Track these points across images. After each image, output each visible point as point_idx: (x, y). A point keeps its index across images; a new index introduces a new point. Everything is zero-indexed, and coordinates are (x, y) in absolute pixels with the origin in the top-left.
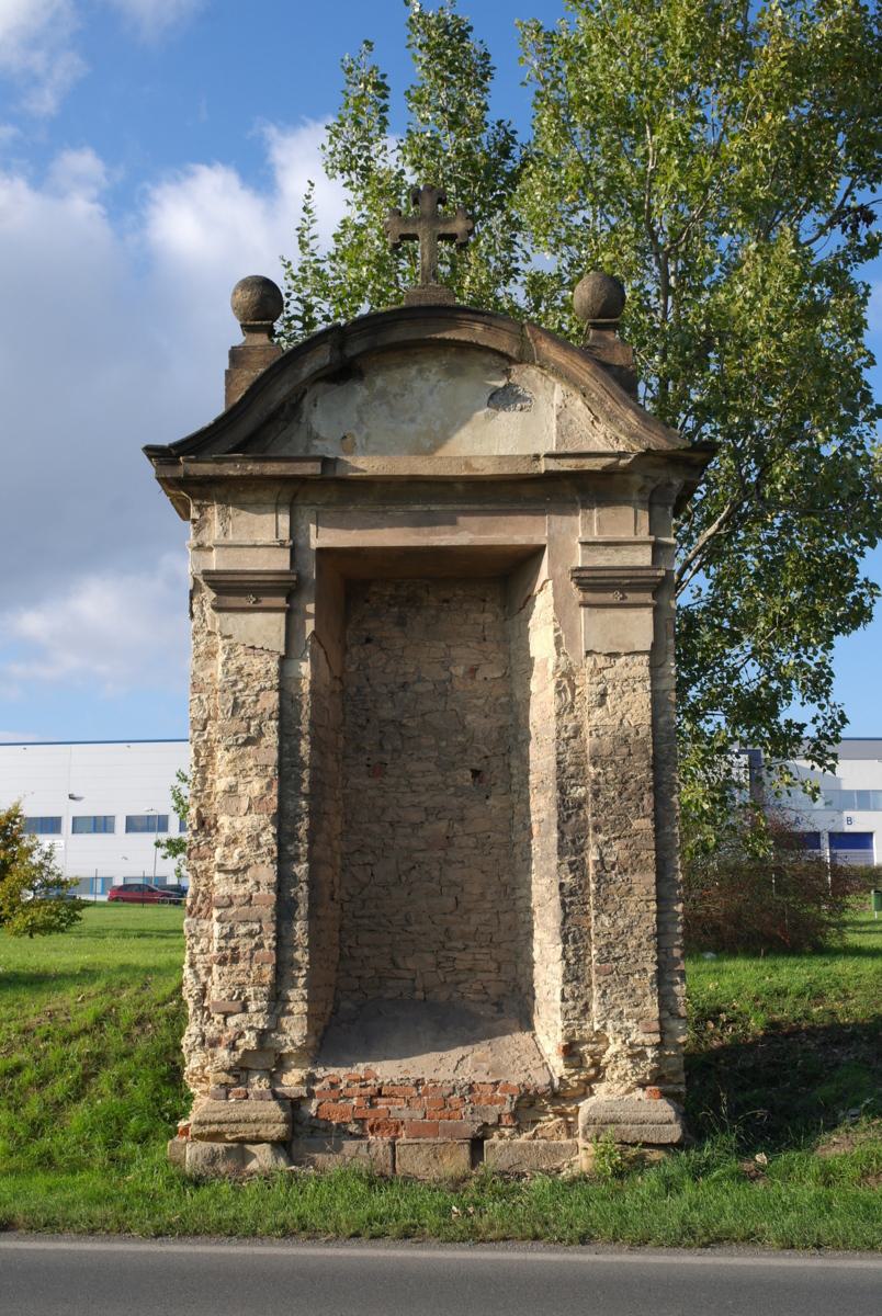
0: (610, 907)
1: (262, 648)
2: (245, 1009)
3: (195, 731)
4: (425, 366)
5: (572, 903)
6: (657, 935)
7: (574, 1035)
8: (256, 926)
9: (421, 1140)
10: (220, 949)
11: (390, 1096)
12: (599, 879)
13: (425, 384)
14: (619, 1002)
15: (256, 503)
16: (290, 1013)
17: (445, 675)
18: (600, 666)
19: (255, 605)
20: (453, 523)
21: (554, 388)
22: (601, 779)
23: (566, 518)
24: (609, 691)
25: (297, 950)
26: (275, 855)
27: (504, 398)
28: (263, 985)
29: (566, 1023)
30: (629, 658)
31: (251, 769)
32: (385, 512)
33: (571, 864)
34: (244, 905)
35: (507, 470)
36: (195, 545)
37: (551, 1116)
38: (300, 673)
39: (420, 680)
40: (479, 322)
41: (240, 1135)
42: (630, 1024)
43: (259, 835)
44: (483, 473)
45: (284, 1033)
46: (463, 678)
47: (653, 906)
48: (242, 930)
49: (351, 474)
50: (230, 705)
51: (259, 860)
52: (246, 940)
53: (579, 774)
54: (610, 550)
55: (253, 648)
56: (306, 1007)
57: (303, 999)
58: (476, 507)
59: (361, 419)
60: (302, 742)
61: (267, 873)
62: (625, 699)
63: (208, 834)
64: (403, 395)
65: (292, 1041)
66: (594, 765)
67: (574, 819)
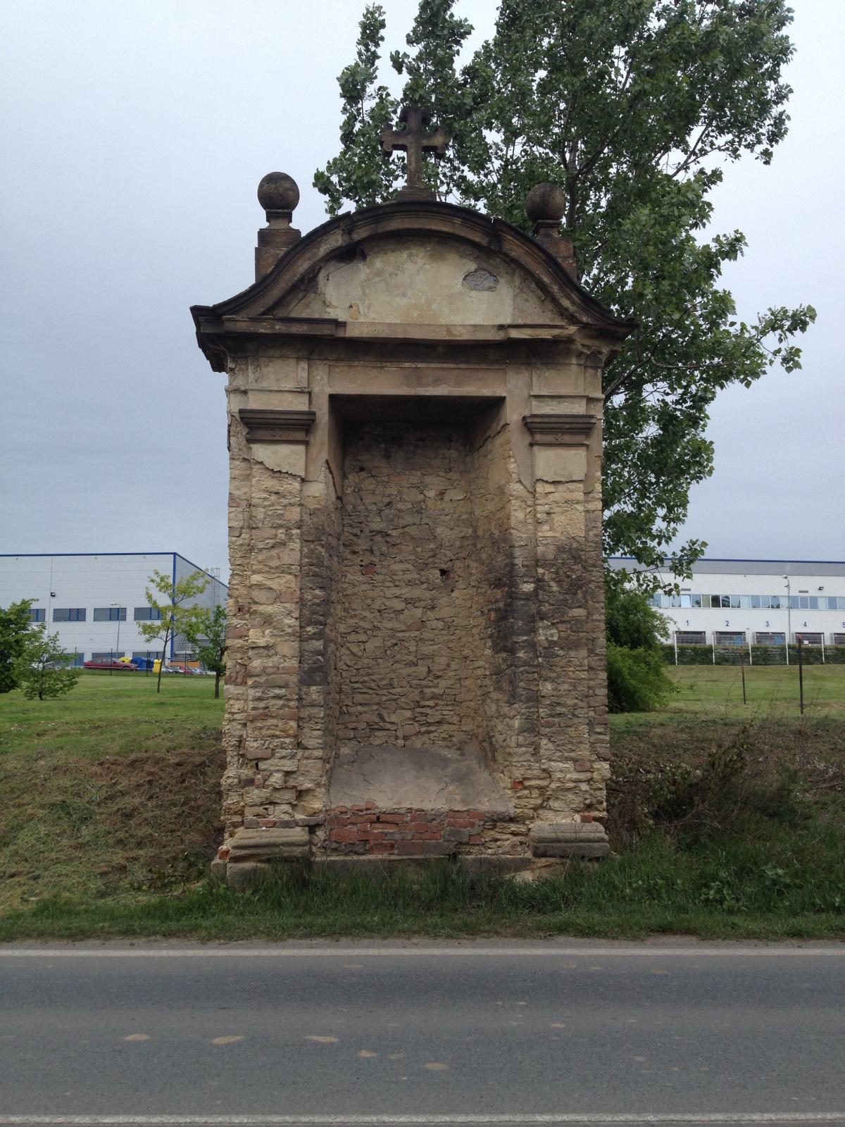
1: (287, 473)
4: (414, 251)
32: (382, 367)
35: (481, 336)
40: (459, 217)
54: (555, 403)
64: (397, 275)
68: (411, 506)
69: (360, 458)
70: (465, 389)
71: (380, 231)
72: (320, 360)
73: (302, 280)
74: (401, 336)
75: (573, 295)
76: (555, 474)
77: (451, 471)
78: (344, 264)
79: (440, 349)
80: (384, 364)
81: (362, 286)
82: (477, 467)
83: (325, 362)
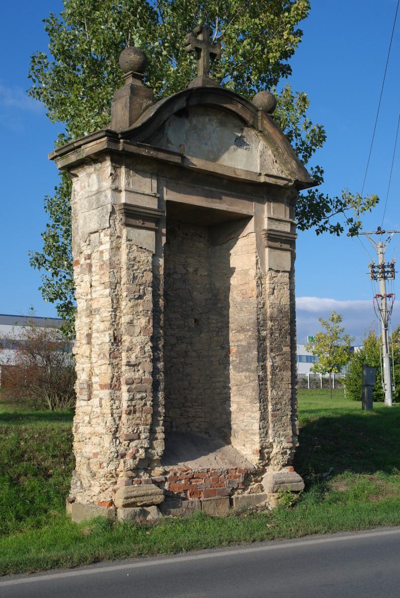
0: (276, 386)
1: (145, 249)
2: (139, 438)
3: (112, 289)
4: (211, 118)
5: (262, 384)
6: (291, 399)
7: (263, 445)
8: (144, 394)
9: (210, 498)
10: (128, 406)
11: (197, 478)
12: (273, 374)
13: (211, 127)
14: (279, 429)
15: (143, 171)
16: (157, 439)
17: (185, 271)
18: (273, 276)
19: (142, 225)
20: (220, 199)
21: (259, 142)
22: (273, 328)
23: (260, 204)
24: (276, 288)
25: (160, 407)
26: (152, 357)
27: (240, 142)
28: (147, 425)
29: (261, 439)
30: (283, 273)
31: (141, 312)
32: (194, 187)
33: (262, 366)
34: (139, 383)
35: (249, 178)
36: (114, 188)
37: (254, 482)
38: (159, 264)
39: (176, 272)
40: (241, 103)
41: (144, 502)
42: (282, 439)
43: (144, 347)
44: (240, 177)
45: (154, 449)
46: (193, 273)
47: (290, 387)
48: (138, 396)
49: (190, 166)
50: (132, 277)
51: (144, 360)
52: (139, 402)
53: (264, 325)
54: (277, 223)
55: (141, 248)
56: (164, 436)
57: (162, 432)
58: (228, 192)
59: (187, 138)
60: (160, 300)
61: (149, 367)
62: (281, 292)
63: (117, 346)
64: (203, 130)
65: (157, 453)
66: (271, 321)
67: (263, 345)
70: (234, 208)
74: (212, 170)
79: (225, 181)
80: (195, 185)
83: (165, 178)
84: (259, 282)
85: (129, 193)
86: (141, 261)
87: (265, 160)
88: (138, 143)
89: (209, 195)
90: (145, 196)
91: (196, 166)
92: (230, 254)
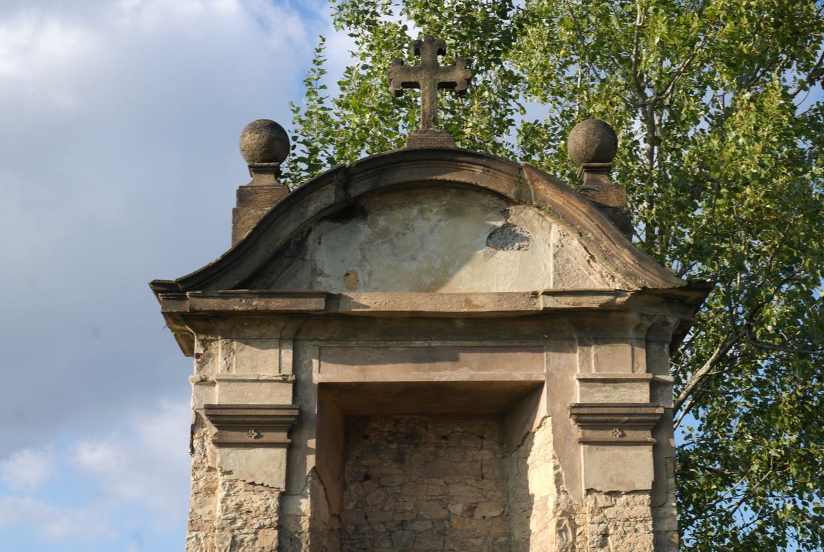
1: (262, 485)
4: (426, 206)
17: (443, 514)
19: (256, 441)
21: (550, 228)
23: (564, 355)
24: (611, 531)
27: (503, 238)
30: (630, 497)
32: (386, 348)
35: (506, 307)
36: (199, 380)
38: (300, 510)
44: (483, 310)
50: (228, 543)
54: (608, 387)
55: (253, 484)
58: (476, 343)
62: (628, 539)
64: (404, 234)
68: (431, 526)
69: (364, 462)
70: (492, 372)
71: (382, 185)
72: (309, 340)
73: (287, 245)
74: (408, 309)
75: (623, 255)
76: (612, 480)
77: (483, 478)
78: (339, 224)
80: (389, 343)
81: (361, 250)
82: (516, 472)
83: (314, 343)
84: (566, 522)
85: (226, 383)
86: (252, 509)
87: (568, 261)
88: (219, 291)
89: (419, 358)
90: (264, 384)
91: (369, 307)
92: (528, 467)
